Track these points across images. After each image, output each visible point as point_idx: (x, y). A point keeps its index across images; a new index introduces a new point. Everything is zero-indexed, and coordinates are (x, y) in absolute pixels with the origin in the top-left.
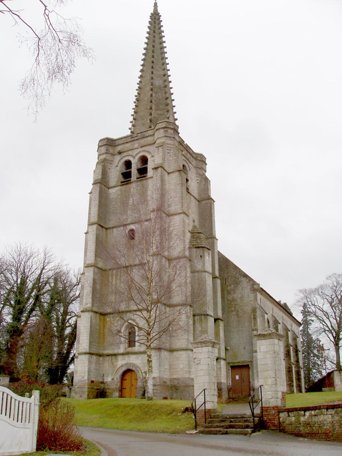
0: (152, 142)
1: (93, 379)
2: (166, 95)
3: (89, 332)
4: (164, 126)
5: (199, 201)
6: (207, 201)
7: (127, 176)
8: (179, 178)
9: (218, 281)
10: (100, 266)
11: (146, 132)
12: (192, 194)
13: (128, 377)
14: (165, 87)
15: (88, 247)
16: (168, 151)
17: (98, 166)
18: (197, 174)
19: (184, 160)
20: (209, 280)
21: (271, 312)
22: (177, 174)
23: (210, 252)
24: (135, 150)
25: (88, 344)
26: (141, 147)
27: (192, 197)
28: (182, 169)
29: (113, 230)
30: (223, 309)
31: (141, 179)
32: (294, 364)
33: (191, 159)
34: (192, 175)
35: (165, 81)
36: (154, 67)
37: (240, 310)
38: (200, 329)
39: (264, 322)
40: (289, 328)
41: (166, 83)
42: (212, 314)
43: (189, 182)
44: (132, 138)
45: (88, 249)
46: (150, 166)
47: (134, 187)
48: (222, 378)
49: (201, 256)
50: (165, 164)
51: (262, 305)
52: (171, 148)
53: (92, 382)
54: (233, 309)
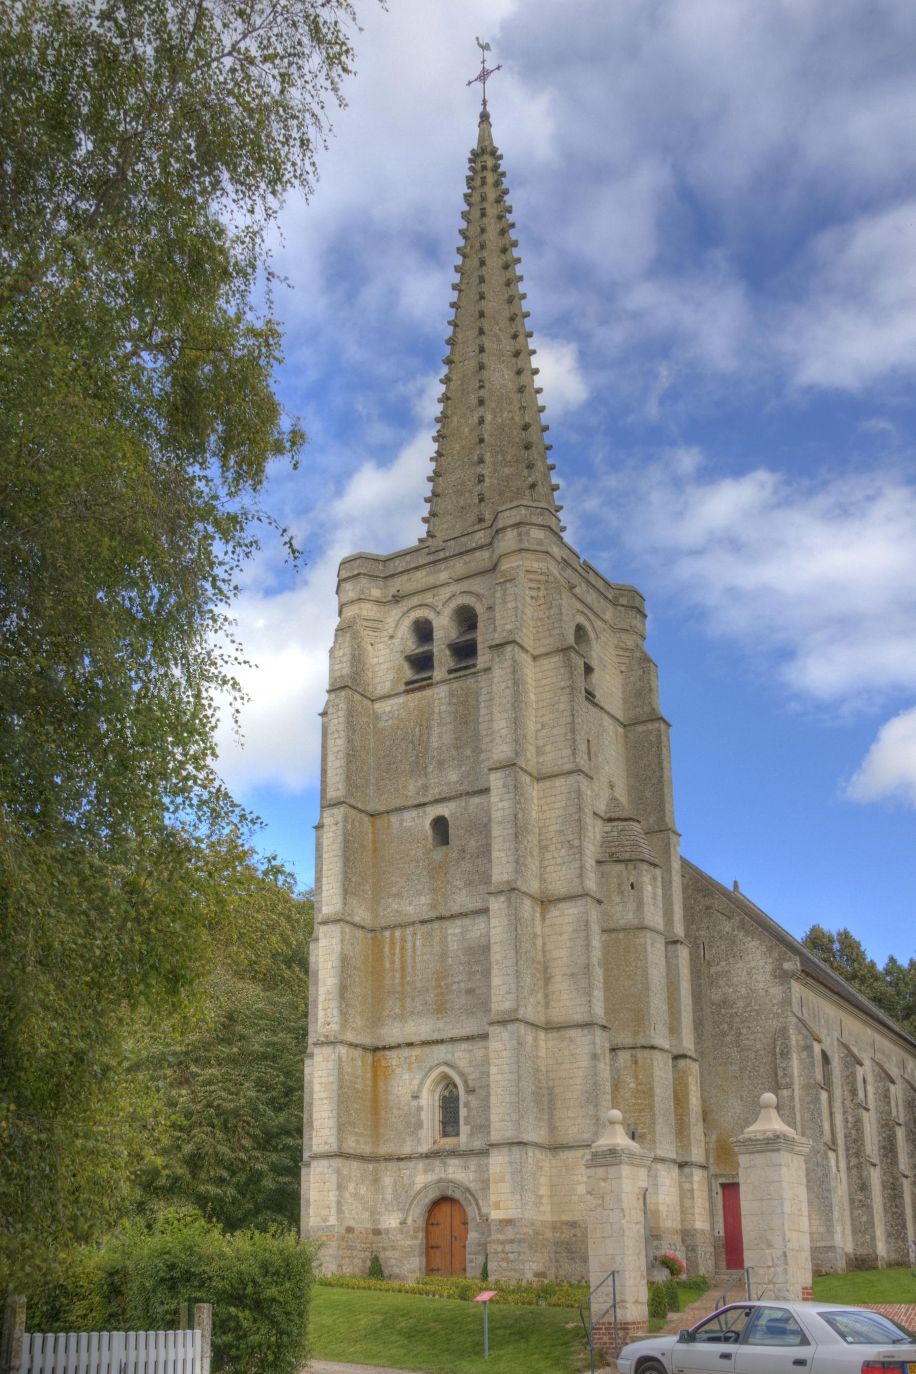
0: (488, 565)
1: (351, 1223)
2: (523, 416)
3: (336, 1099)
4: (517, 519)
5: (625, 726)
6: (650, 726)
7: (422, 663)
8: (562, 670)
9: (684, 953)
10: (357, 919)
11: (470, 537)
12: (606, 707)
13: (445, 1208)
14: (521, 390)
15: (325, 868)
16: (534, 593)
17: (340, 640)
18: (617, 647)
19: (578, 611)
20: (655, 951)
21: (836, 1034)
22: (557, 659)
23: (658, 872)
24: (442, 590)
25: (334, 1131)
26: (458, 580)
27: (606, 718)
28: (571, 640)
29: (389, 820)
30: (698, 1025)
31: (461, 673)
32: (906, 1177)
33: (599, 604)
34: (604, 652)
35: (519, 372)
36: (486, 328)
37: (744, 1031)
38: (632, 1085)
39: (812, 1064)
40: (894, 1072)
41: (523, 380)
42: (667, 1046)
43: (595, 676)
44: (429, 554)
45: (325, 873)
46: (483, 637)
47: (439, 695)
48: (697, 1217)
49: (632, 886)
50: (524, 630)
51: (806, 1017)
52: (539, 581)
53: (350, 1230)
54: (726, 1027)
